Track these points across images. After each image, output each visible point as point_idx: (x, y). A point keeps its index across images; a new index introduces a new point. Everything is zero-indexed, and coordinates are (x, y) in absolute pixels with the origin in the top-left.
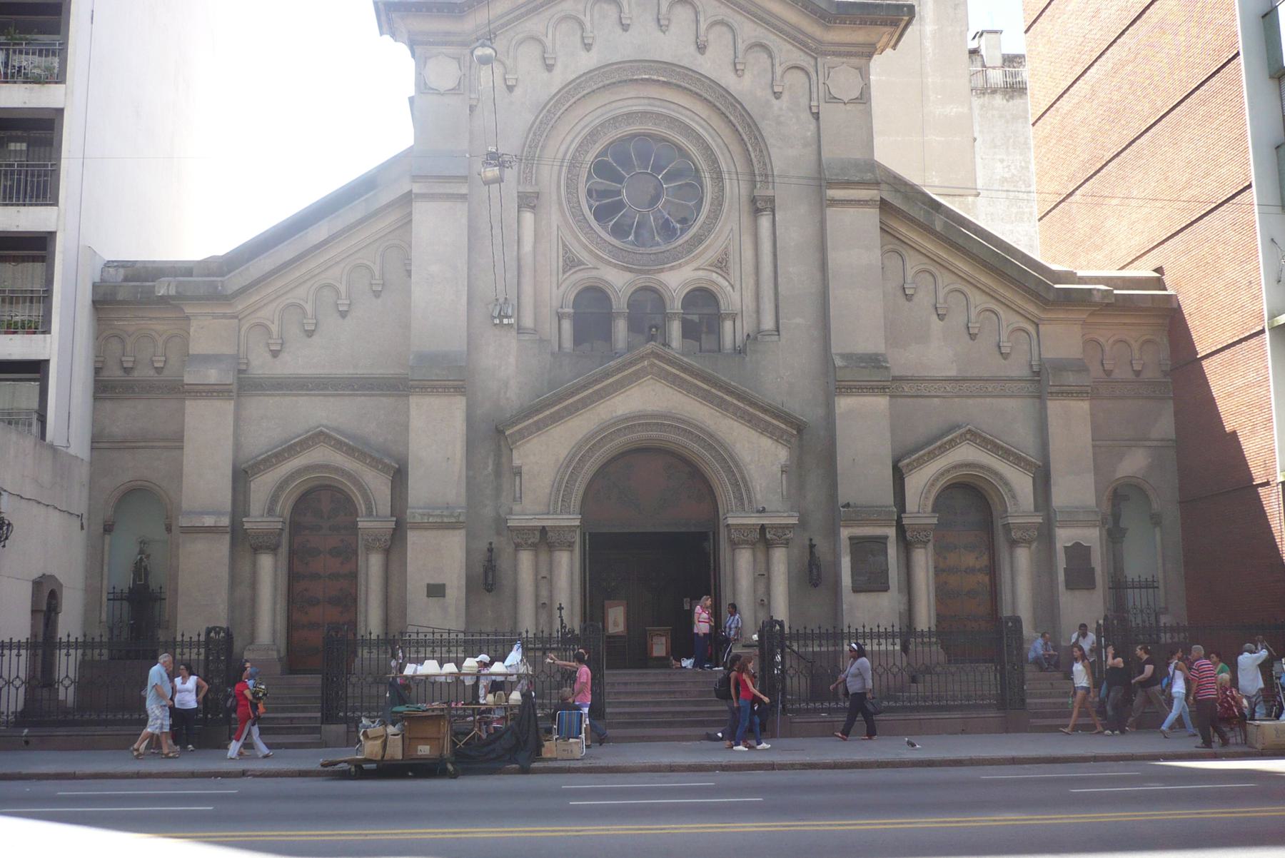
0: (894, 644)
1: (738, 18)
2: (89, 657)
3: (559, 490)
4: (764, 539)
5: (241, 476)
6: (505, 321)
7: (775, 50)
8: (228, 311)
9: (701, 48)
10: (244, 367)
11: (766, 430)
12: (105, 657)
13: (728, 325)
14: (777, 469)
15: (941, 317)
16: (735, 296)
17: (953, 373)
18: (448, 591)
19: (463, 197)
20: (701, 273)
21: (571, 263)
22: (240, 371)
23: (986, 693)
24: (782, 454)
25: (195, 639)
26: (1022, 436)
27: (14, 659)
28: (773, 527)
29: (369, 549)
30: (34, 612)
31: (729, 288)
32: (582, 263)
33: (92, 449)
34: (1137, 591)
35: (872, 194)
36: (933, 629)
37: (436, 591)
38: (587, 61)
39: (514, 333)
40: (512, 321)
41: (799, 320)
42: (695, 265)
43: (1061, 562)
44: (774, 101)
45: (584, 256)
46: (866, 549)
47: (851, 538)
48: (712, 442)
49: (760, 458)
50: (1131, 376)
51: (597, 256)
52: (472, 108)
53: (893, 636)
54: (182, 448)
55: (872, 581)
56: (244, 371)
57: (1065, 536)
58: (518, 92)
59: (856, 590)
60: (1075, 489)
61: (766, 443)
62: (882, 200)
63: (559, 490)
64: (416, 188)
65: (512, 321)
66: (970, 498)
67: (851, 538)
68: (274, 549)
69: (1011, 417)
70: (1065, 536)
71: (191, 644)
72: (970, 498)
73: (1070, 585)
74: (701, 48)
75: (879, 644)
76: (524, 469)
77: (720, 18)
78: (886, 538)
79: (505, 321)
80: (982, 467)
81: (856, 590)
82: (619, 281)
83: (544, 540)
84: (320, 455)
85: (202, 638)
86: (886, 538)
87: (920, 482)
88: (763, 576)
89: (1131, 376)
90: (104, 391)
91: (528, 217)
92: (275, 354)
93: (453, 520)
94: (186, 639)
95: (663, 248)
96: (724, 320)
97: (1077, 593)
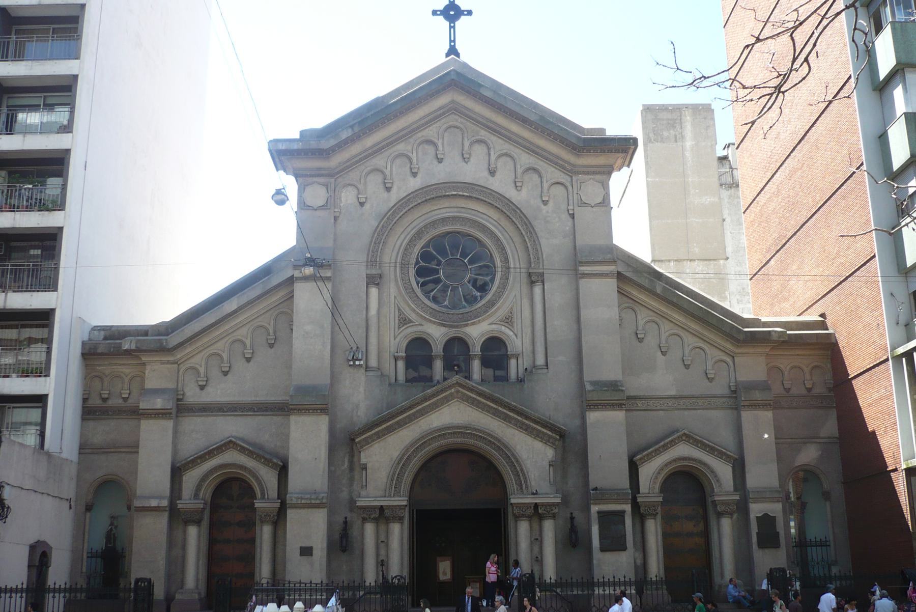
1: (517, 151)
4: (537, 513)
6: (357, 363)
10: (181, 397)
11: (538, 436)
13: (513, 362)
14: (546, 464)
16: (518, 342)
17: (673, 392)
18: (314, 552)
21: (404, 321)
22: (178, 400)
24: (550, 453)
28: (543, 504)
30: (30, 566)
32: (410, 321)
37: (306, 551)
38: (414, 184)
39: (363, 371)
41: (561, 358)
45: (413, 316)
46: (610, 520)
49: (533, 455)
52: (336, 218)
54: (137, 452)
55: (614, 542)
57: (756, 509)
59: (603, 549)
60: (763, 474)
61: (538, 445)
66: (687, 483)
67: (599, 512)
68: (198, 523)
70: (756, 509)
76: (369, 466)
79: (357, 363)
80: (695, 460)
81: (603, 549)
82: (437, 334)
83: (382, 515)
87: (649, 472)
88: (537, 540)
90: (88, 414)
91: (374, 291)
92: (202, 388)
93: (318, 502)
97: (767, 551)
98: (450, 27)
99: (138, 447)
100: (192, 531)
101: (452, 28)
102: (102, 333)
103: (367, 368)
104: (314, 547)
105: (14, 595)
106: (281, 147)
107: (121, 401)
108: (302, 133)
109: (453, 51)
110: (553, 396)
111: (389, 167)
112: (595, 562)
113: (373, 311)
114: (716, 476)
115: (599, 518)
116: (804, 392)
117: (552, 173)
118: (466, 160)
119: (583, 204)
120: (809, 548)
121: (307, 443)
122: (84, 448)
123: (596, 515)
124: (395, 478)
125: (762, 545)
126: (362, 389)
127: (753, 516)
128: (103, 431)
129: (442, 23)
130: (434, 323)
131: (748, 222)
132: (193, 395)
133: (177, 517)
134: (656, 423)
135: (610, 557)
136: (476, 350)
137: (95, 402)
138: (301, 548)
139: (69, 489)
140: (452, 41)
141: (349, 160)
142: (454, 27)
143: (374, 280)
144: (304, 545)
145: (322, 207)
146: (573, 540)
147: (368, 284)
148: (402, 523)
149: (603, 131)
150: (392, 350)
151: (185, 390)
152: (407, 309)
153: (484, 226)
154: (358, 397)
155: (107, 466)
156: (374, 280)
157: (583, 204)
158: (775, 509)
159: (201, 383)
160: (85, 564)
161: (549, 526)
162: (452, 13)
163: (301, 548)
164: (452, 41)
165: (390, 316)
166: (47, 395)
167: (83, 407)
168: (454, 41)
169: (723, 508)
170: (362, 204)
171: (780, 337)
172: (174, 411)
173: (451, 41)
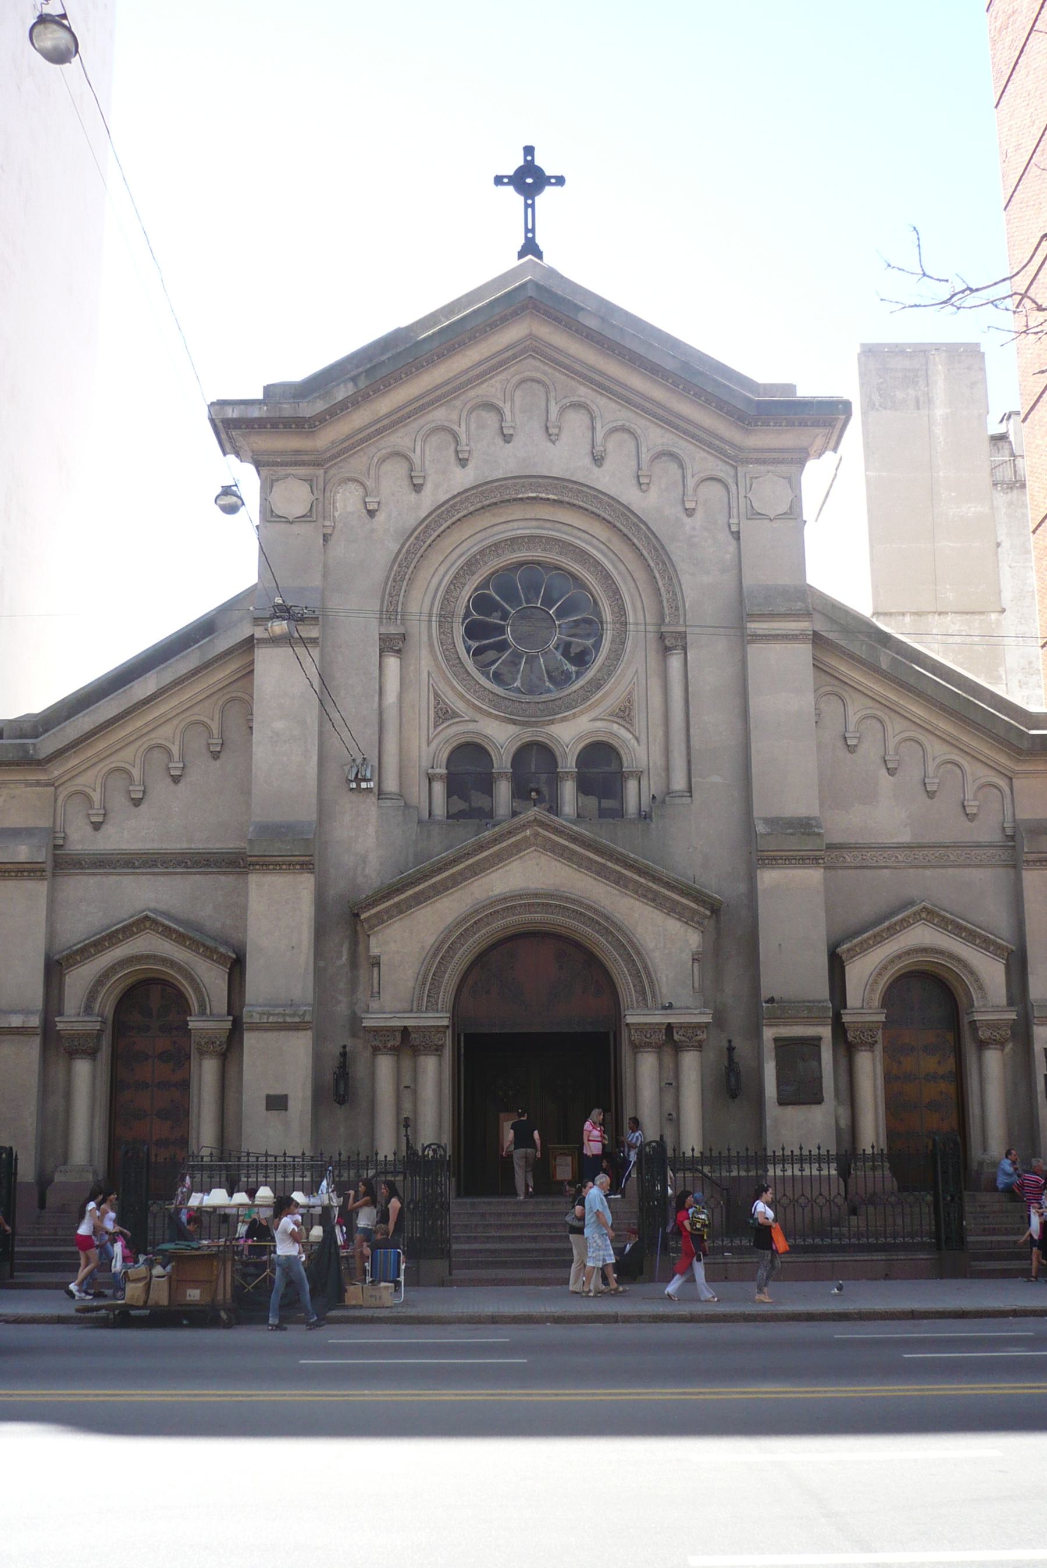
1: (643, 423)
4: (671, 1041)
5: (55, 969)
8: (42, 777)
10: (61, 842)
11: (672, 909)
13: (632, 785)
14: (687, 957)
16: (641, 751)
17: (906, 838)
18: (291, 1103)
21: (444, 714)
22: (56, 847)
24: (693, 939)
28: (681, 1026)
31: (633, 742)
32: (455, 715)
35: (804, 625)
38: (462, 478)
39: (373, 799)
40: (372, 784)
41: (716, 779)
45: (459, 706)
46: (795, 1054)
47: (776, 1040)
48: (607, 925)
49: (665, 945)
52: (326, 538)
55: (801, 1091)
58: (381, 517)
59: (782, 1102)
61: (674, 926)
65: (372, 784)
67: (776, 1040)
68: (92, 1054)
76: (384, 959)
78: (819, 1039)
79: (364, 785)
81: (782, 1102)
82: (501, 736)
83: (406, 1043)
84: (922, 935)
86: (819, 1039)
87: (864, 973)
88: (671, 1085)
91: (392, 663)
92: (97, 826)
93: (297, 1020)
98: (527, 206)
100: (82, 1068)
101: (530, 206)
103: (381, 794)
106: (232, 413)
108: (268, 390)
115: (778, 1048)
118: (552, 437)
121: (278, 920)
124: (429, 980)
130: (496, 717)
132: (81, 839)
135: (792, 1113)
140: (530, 230)
143: (393, 644)
144: (272, 1092)
146: (732, 1084)
149: (791, 388)
151: (68, 832)
152: (450, 694)
153: (584, 552)
154: (365, 842)
156: (393, 644)
161: (690, 1062)
164: (530, 230)
165: (418, 706)
168: (533, 231)
170: (371, 513)
173: (527, 230)
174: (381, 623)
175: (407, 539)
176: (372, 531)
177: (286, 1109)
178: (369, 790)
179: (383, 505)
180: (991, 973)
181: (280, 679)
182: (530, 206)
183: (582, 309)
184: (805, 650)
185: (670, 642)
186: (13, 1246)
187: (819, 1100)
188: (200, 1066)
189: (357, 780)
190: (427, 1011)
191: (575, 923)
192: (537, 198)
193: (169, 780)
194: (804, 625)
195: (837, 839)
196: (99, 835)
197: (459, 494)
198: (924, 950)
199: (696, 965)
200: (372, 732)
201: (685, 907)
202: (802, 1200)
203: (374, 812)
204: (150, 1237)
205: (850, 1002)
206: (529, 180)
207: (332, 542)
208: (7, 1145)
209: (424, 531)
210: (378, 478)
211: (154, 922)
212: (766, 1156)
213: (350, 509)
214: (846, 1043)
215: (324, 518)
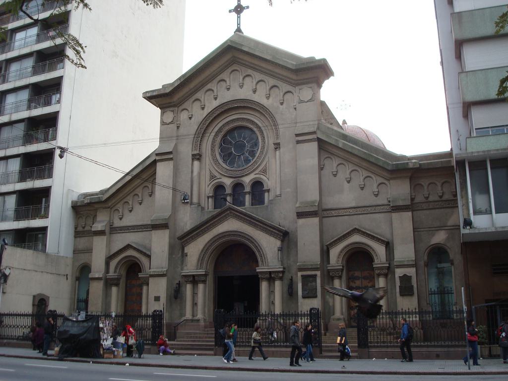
0: (416, 317)
1: (267, 77)
2: (462, 315)
3: (265, 258)
4: (271, 278)
5: (325, 252)
6: (186, 201)
7: (278, 85)
8: (107, 206)
9: (255, 91)
10: (111, 224)
11: (271, 234)
12: (431, 318)
13: (266, 194)
14: (276, 249)
15: (349, 182)
16: (269, 183)
17: (353, 205)
18: (161, 298)
19: (171, 159)
20: (257, 176)
21: (213, 177)
22: (111, 225)
23: (372, 340)
24: (278, 243)
25: (306, 313)
26: (383, 230)
27: (141, 321)
28: (274, 272)
29: (379, 275)
30: (33, 305)
31: (267, 180)
32: (216, 177)
33: (74, 253)
34: (433, 295)
35: (314, 136)
36: (123, 314)
37: (157, 299)
38: (216, 104)
39: (189, 205)
40: (188, 201)
41: (288, 190)
42: (255, 173)
43: (398, 284)
44: (281, 106)
45: (216, 174)
46: (308, 280)
47: (302, 276)
48: (250, 239)
49: (269, 245)
50: (424, 200)
51: (221, 174)
52: (178, 127)
53: (416, 313)
54: (92, 252)
55: (310, 294)
56: (112, 225)
57: (399, 272)
58: (193, 119)
59: (304, 297)
60: (405, 251)
61: (272, 239)
62: (318, 138)
63: (265, 258)
64: (158, 158)
65: (188, 201)
66: (359, 258)
67: (302, 276)
68: (117, 285)
69: (378, 223)
70: (399, 272)
71: (304, 315)
72: (359, 258)
73: (402, 294)
74: (255, 91)
75: (409, 317)
76: (188, 254)
77: (260, 79)
78: (316, 275)
79: (186, 201)
80: (363, 243)
81: (304, 297)
82: (228, 182)
83: (194, 280)
84: (356, 238)
85: (308, 313)
86: (316, 275)
87: (335, 253)
88: (271, 292)
89: (424, 200)
90: (77, 235)
91: (196, 163)
92: (121, 219)
93: (162, 273)
94: (303, 313)
95: (245, 167)
96: (265, 192)
97: (405, 297)
98: (238, 17)
99: (92, 250)
100: (114, 289)
101: (239, 17)
102: (83, 196)
103: (192, 203)
104: (161, 296)
105: (25, 317)
106: (148, 95)
107: (90, 228)
108: (163, 86)
109: (239, 30)
110: (282, 214)
111: (203, 97)
112: (299, 304)
113: (195, 173)
114: (375, 253)
115: (303, 279)
116: (437, 198)
117: (286, 87)
118: (241, 87)
119: (301, 102)
120: (446, 295)
121: (159, 244)
122: (76, 251)
123: (398, 278)
124: (201, 260)
125: (402, 294)
126: (188, 214)
127: (397, 276)
128: (83, 242)
129: (234, 15)
130: (227, 176)
131: (398, 98)
132: (117, 223)
133: (109, 283)
134: (341, 225)
135: (307, 301)
136: (248, 189)
137: (80, 229)
138: (155, 297)
139: (69, 271)
140: (239, 24)
141: (183, 96)
142: (240, 17)
143: (197, 157)
144: (156, 295)
145: (171, 123)
146: (290, 293)
147: (193, 159)
148: (205, 284)
149: (313, 58)
150: (207, 193)
151: (114, 221)
152: (214, 170)
153: (253, 121)
154: (187, 219)
155: (83, 259)
156: (197, 157)
157: (301, 102)
158: (411, 272)
159: (120, 217)
160: (76, 305)
161: (278, 284)
162: (239, 9)
163: (155, 297)
164: (239, 24)
165: (203, 175)
166: (47, 227)
167: (75, 232)
168: (240, 24)
169: (379, 271)
170: (190, 118)
171: (414, 165)
172: (107, 231)
173: (238, 24)
174: (192, 151)
175: (200, 125)
176: (190, 123)
177: (159, 301)
178: (187, 202)
179: (196, 113)
180: (380, 251)
181: (164, 171)
182: (239, 17)
183: (243, 45)
184: (315, 145)
185: (277, 146)
186: (321, 344)
187: (316, 297)
188: (378, 280)
189: (184, 199)
190: (200, 269)
191: (221, 241)
192: (241, 14)
193: (139, 204)
194: (314, 136)
195: (330, 207)
196: (121, 221)
197: (214, 109)
198: (357, 243)
199: (279, 252)
200: (189, 184)
201: (275, 233)
202: (277, 330)
203: (189, 208)
204: (369, 340)
205: (331, 262)
206: (239, 9)
207: (180, 128)
208: (317, 307)
209: (206, 121)
210: (192, 107)
211: (131, 246)
212: (419, 315)
213: (185, 118)
214: (329, 276)
215: (177, 122)
